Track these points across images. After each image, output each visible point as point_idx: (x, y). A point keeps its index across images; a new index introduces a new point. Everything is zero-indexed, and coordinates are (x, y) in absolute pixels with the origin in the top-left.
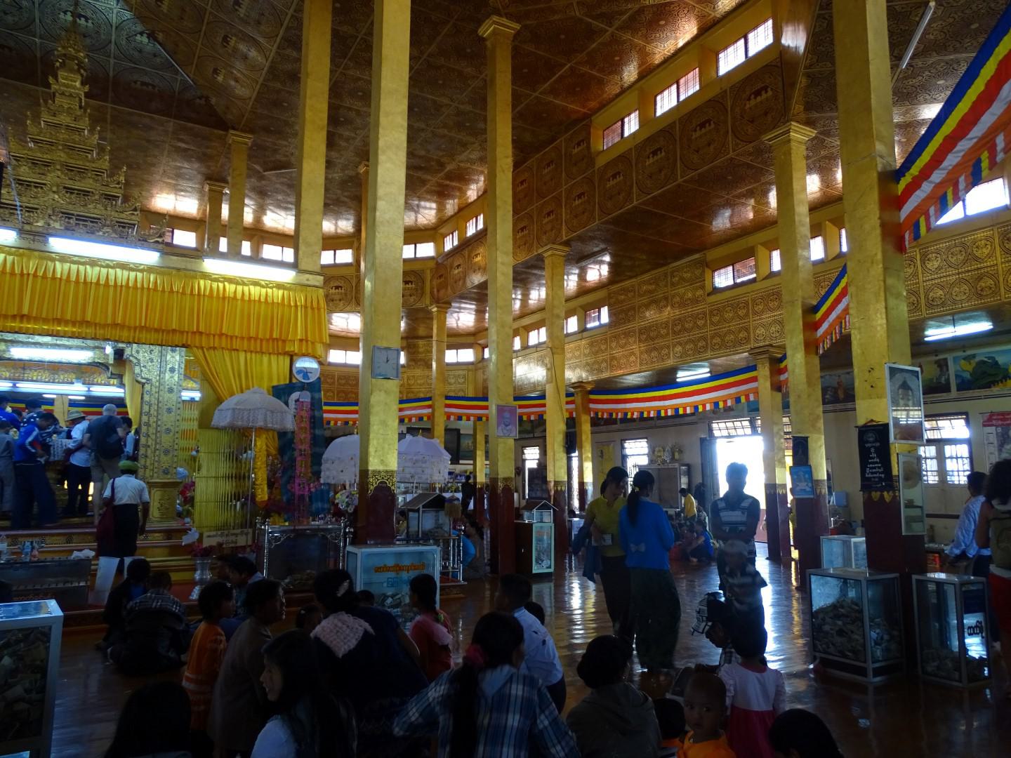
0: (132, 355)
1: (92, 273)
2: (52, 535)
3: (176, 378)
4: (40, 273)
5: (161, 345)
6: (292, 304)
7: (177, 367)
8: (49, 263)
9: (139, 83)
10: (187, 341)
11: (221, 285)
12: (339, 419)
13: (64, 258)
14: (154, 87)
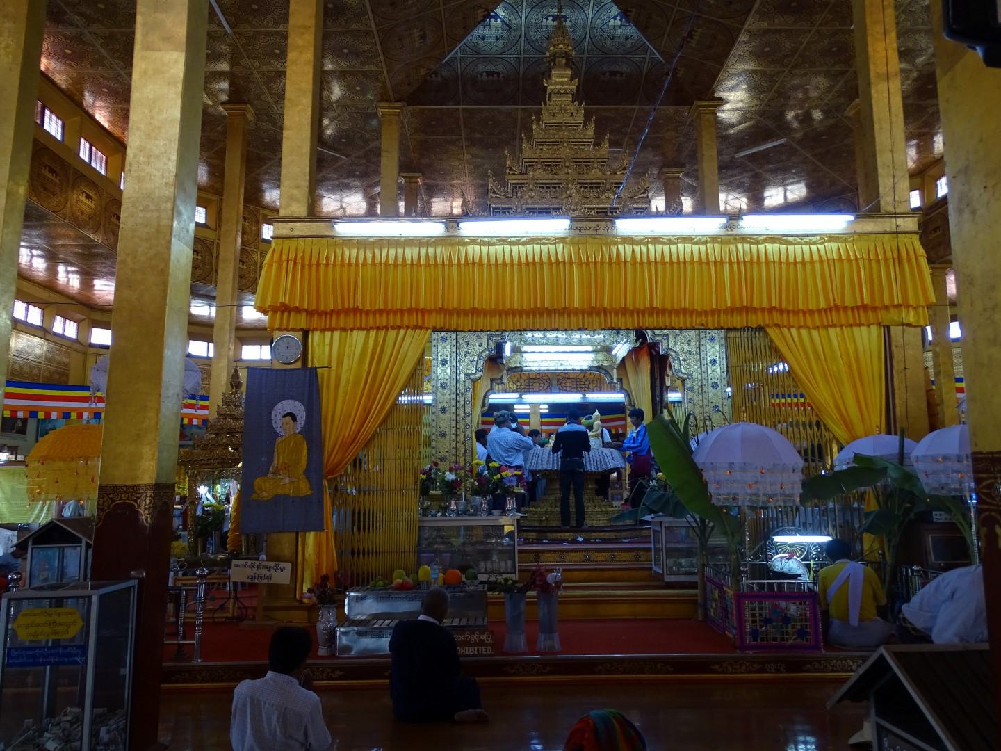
0: (669, 349)
1: (801, 251)
2: (87, 619)
3: (448, 371)
4: (455, 261)
5: (456, 331)
6: (852, 258)
7: (448, 359)
8: (461, 248)
9: (608, 74)
10: (638, 323)
11: (637, 248)
12: (55, 409)
13: (629, 240)
14: (498, 74)
